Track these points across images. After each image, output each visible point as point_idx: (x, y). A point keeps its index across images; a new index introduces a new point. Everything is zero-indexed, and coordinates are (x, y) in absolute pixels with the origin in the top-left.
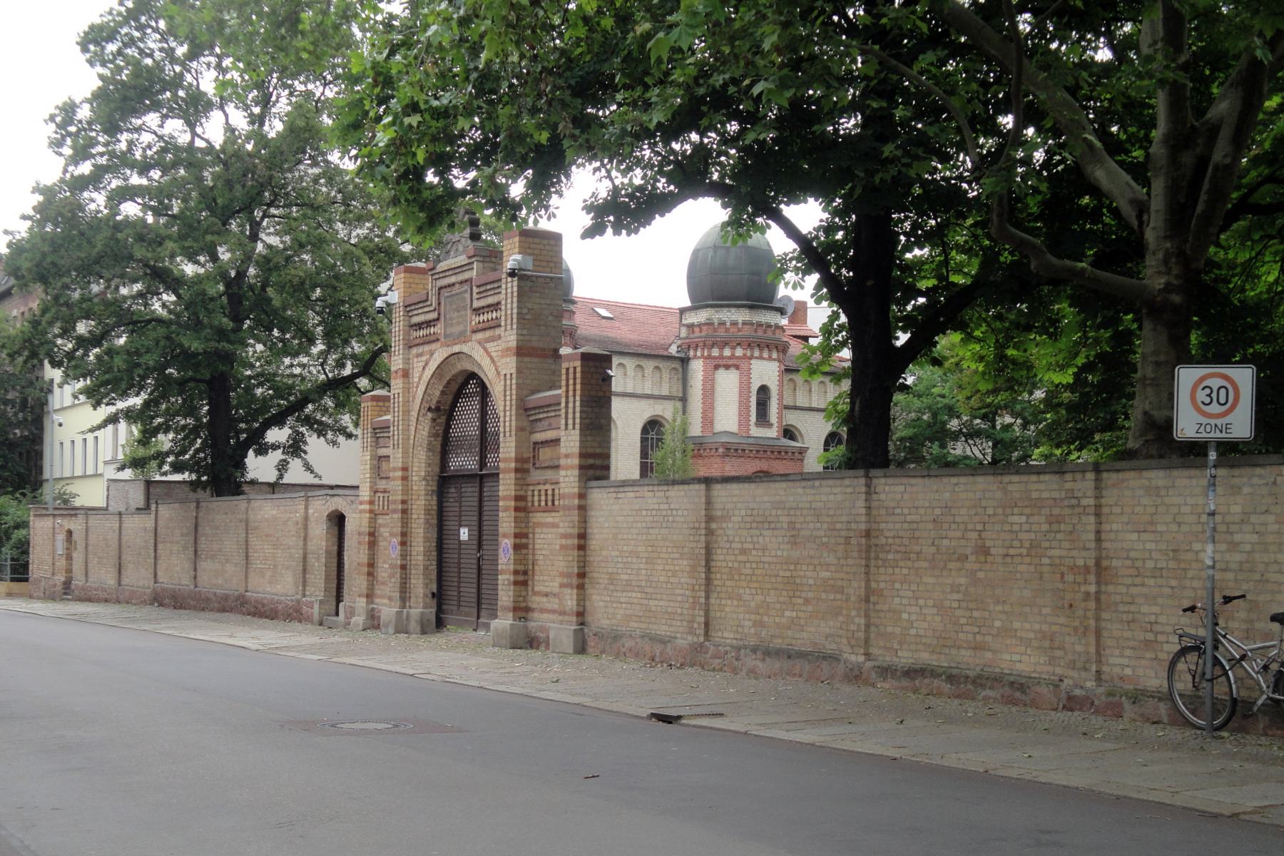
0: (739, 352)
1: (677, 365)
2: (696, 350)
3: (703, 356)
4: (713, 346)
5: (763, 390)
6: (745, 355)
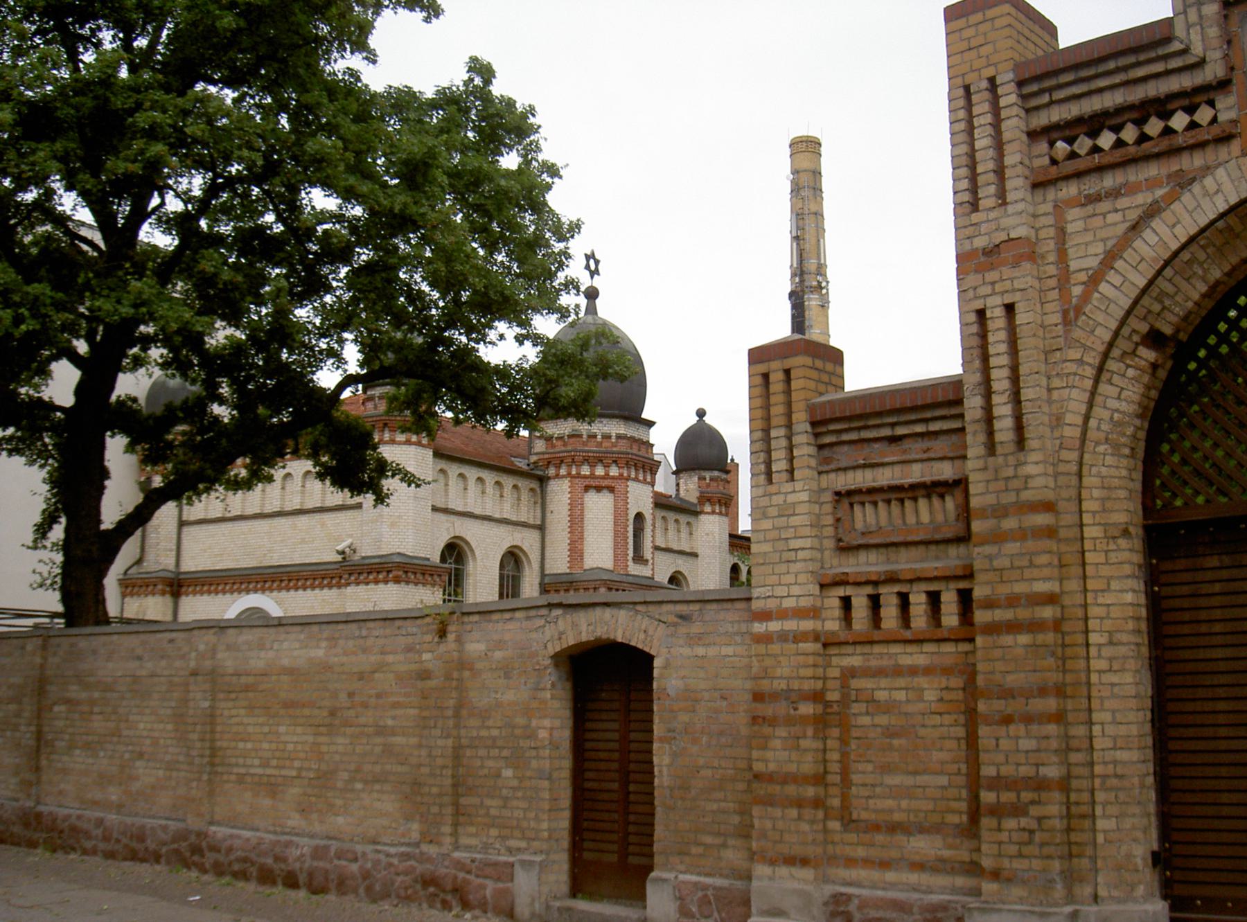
0: (614, 471)
2: (558, 467)
3: (569, 475)
4: (582, 463)
5: (639, 517)
6: (621, 475)
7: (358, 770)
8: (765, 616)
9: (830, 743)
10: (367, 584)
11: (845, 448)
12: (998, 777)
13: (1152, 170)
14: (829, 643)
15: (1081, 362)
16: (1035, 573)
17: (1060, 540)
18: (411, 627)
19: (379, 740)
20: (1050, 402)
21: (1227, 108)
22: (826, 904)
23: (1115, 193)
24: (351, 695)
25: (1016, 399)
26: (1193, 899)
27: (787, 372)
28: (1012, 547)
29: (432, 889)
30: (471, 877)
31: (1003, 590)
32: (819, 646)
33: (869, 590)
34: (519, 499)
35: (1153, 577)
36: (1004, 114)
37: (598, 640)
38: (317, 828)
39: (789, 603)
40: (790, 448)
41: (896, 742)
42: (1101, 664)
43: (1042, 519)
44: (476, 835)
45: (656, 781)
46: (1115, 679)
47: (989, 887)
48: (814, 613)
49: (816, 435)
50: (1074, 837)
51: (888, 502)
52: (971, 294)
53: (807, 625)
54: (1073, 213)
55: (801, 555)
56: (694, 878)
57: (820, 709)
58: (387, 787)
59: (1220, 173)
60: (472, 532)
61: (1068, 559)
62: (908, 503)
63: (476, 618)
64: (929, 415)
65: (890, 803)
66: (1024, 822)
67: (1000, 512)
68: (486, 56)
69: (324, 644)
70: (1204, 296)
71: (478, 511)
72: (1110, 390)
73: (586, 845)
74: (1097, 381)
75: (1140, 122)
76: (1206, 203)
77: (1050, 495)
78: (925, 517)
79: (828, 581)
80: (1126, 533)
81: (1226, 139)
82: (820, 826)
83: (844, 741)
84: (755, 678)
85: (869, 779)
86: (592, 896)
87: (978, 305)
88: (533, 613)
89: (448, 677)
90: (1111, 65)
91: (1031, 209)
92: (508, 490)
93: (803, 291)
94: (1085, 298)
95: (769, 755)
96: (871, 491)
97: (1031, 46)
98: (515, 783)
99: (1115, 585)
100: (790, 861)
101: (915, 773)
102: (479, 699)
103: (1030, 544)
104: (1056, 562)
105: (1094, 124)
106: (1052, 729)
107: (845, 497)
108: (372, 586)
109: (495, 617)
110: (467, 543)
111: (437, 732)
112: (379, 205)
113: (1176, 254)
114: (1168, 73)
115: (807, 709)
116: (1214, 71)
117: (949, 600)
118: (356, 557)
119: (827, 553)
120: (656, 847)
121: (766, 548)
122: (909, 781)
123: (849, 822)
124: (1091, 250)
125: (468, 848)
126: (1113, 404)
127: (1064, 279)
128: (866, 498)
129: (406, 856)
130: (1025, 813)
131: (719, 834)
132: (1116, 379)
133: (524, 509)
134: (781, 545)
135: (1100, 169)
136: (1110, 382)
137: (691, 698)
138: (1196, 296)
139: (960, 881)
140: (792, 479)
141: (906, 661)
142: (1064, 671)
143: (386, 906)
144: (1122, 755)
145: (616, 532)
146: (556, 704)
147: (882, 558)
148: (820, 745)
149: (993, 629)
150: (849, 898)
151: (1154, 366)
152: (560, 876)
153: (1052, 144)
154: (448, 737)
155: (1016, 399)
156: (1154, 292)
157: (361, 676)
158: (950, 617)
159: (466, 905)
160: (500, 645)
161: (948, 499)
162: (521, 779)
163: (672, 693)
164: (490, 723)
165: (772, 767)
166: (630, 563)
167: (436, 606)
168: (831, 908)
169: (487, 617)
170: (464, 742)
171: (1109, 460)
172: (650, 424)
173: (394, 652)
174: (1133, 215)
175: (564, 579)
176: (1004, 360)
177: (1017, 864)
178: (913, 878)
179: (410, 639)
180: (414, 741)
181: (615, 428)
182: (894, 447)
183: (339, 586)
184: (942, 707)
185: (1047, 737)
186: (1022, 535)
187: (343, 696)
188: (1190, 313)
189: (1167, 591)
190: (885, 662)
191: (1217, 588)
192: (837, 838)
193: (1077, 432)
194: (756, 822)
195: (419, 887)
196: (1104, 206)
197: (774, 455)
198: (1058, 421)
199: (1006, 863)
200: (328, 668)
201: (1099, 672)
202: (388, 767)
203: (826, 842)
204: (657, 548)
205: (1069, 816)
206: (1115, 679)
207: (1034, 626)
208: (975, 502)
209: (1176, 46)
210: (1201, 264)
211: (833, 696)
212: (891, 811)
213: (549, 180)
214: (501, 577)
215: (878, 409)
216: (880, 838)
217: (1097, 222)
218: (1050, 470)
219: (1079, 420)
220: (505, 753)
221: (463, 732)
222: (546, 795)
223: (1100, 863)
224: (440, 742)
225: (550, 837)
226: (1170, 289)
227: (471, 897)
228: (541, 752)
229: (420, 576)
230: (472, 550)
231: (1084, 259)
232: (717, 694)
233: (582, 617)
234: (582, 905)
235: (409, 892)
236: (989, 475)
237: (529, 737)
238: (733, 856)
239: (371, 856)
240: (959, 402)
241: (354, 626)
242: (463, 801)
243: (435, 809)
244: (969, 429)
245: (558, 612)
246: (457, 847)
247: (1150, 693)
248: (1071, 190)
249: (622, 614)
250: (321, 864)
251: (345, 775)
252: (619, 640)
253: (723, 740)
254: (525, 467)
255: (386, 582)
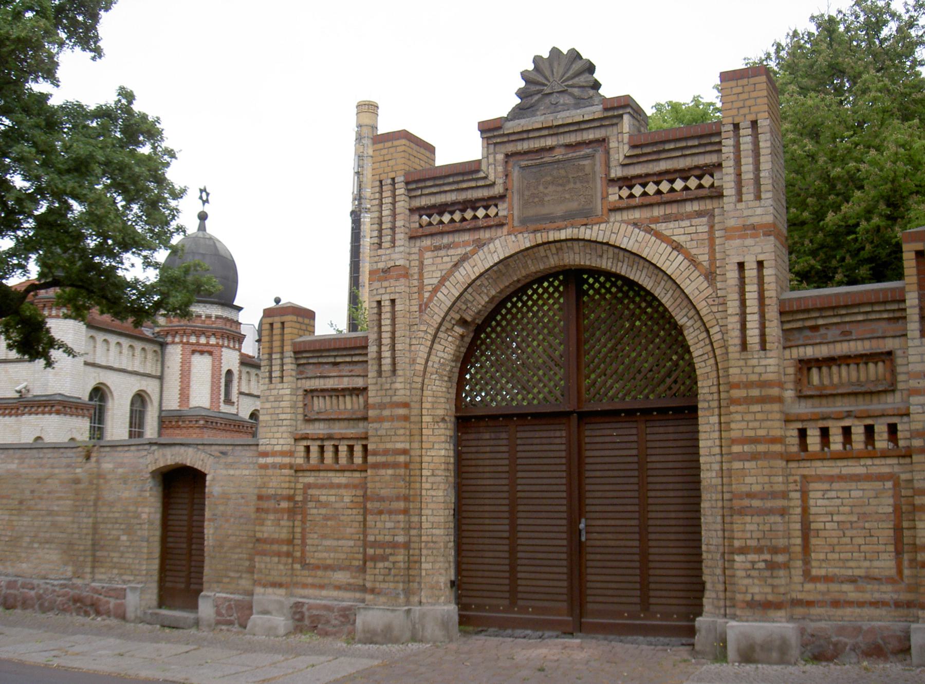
0: (213, 341)
1: (157, 348)
2: (174, 336)
3: (181, 342)
4: (191, 335)
5: (229, 373)
6: (218, 343)
7: (35, 536)
8: (265, 454)
9: (297, 523)
10: (37, 414)
11: (311, 367)
12: (375, 541)
13: (466, 237)
14: (298, 470)
15: (426, 332)
16: (397, 438)
17: (410, 423)
18: (69, 453)
19: (49, 518)
20: (410, 351)
21: (503, 209)
22: (291, 607)
23: (448, 247)
24: (32, 492)
25: (393, 349)
26: (470, 605)
27: (283, 323)
28: (386, 425)
29: (78, 604)
30: (101, 597)
31: (382, 446)
32: (293, 471)
33: (319, 443)
34: (145, 358)
35: (458, 443)
36: (397, 199)
37: (177, 464)
38: (10, 570)
39: (278, 448)
40: (282, 365)
41: (329, 523)
42: (428, 486)
43: (401, 411)
44: (105, 573)
45: (206, 543)
46: (433, 493)
47: (369, 597)
48: (291, 454)
49: (297, 359)
50: (411, 572)
51: (331, 397)
52: (375, 292)
53: (287, 460)
54: (428, 254)
55: (285, 423)
56: (224, 595)
57: (292, 505)
58: (53, 546)
59: (497, 242)
60: (112, 380)
61: (414, 432)
62: (341, 398)
63: (108, 449)
64: (352, 352)
65: (325, 555)
66: (387, 564)
67: (382, 406)
68: (129, 87)
69: (16, 461)
70: (487, 303)
71: (116, 366)
72: (439, 347)
73: (168, 579)
74: (433, 342)
75: (463, 211)
76: (489, 257)
77: (407, 399)
78: (349, 406)
79: (298, 437)
80: (443, 420)
81: (501, 225)
82: (290, 567)
83: (303, 522)
84: (259, 488)
85: (316, 542)
86: (170, 607)
87: (378, 298)
88: (141, 447)
89: (91, 483)
90: (451, 180)
91: (407, 250)
92: (138, 351)
93: (360, 211)
94: (430, 299)
95: (265, 529)
96: (323, 390)
97: (417, 161)
98: (128, 544)
99: (436, 446)
100: (275, 585)
101: (338, 539)
102: (108, 496)
103: (397, 424)
104: (408, 433)
105: (441, 209)
106: (401, 517)
107: (310, 393)
108: (40, 416)
109: (119, 449)
110: (108, 387)
111: (84, 514)
112: (57, 188)
113: (474, 281)
114: (477, 187)
115: (284, 505)
116: (498, 190)
117: (358, 449)
118: (30, 396)
119: (299, 422)
120: (205, 579)
121: (267, 418)
122: (335, 543)
123: (305, 565)
124: (434, 275)
125: (100, 581)
126: (441, 354)
127: (421, 288)
128: (320, 394)
129: (63, 586)
130: (387, 560)
131: (238, 571)
132: (443, 342)
133: (149, 364)
134: (275, 417)
135: (442, 233)
136: (439, 343)
137: (225, 497)
138: (483, 303)
139: (358, 595)
140: (282, 382)
141: (336, 481)
142: (409, 489)
143: (51, 614)
144: (435, 531)
145: (213, 382)
146: (153, 499)
147: (327, 426)
148: (291, 524)
149: (376, 466)
150: (303, 604)
151: (462, 336)
152: (152, 595)
153: (421, 216)
154: (90, 517)
155: (393, 349)
156: (463, 299)
157: (39, 481)
158: (358, 460)
159: (98, 613)
160: (121, 465)
161: (360, 397)
162: (131, 541)
163: (216, 494)
164: (114, 509)
165: (266, 535)
166: (222, 404)
167: (85, 441)
168: (294, 609)
169: (115, 449)
170: (99, 520)
171: (437, 383)
172: (239, 309)
173: (59, 467)
174: (455, 259)
175: (175, 414)
176: (389, 328)
177: (383, 586)
178: (335, 593)
179: (69, 460)
180: (70, 519)
181: (215, 311)
182: (336, 368)
183: (17, 415)
184: (352, 505)
185: (399, 522)
186: (392, 418)
187: (27, 492)
188: (480, 311)
189: (465, 450)
190: (325, 481)
191: (488, 449)
192: (298, 573)
193: (422, 368)
194: (257, 565)
195: (71, 603)
196: (442, 253)
197: (274, 368)
198: (413, 361)
199: (377, 585)
200: (18, 475)
201: (427, 490)
202: (54, 534)
203: (292, 575)
204: (241, 393)
205: (409, 561)
206: (433, 493)
207: (395, 465)
208: (371, 401)
209: (482, 175)
210: (486, 287)
211: (299, 498)
212: (325, 559)
213: (169, 160)
214: (132, 411)
215: (327, 347)
216: (320, 573)
217: (439, 260)
218: (408, 386)
219: (423, 362)
220: (123, 526)
221: (99, 514)
222: (145, 550)
223: (423, 585)
224: (85, 520)
225: (147, 574)
226: (471, 298)
227: (101, 608)
228: (143, 526)
229: (74, 410)
230: (111, 392)
231: (431, 279)
232: (239, 496)
233: (168, 451)
234: (165, 612)
235: (66, 606)
236: (378, 387)
237: (136, 518)
238: (245, 583)
239: (43, 586)
240: (366, 347)
241: (35, 451)
242: (98, 554)
243: (81, 559)
244: (370, 362)
245: (155, 448)
246: (94, 580)
247: (453, 501)
248: (427, 242)
249: (190, 450)
250: (12, 591)
251: (28, 539)
252: (188, 464)
253: (242, 521)
254: (151, 336)
255: (50, 413)
